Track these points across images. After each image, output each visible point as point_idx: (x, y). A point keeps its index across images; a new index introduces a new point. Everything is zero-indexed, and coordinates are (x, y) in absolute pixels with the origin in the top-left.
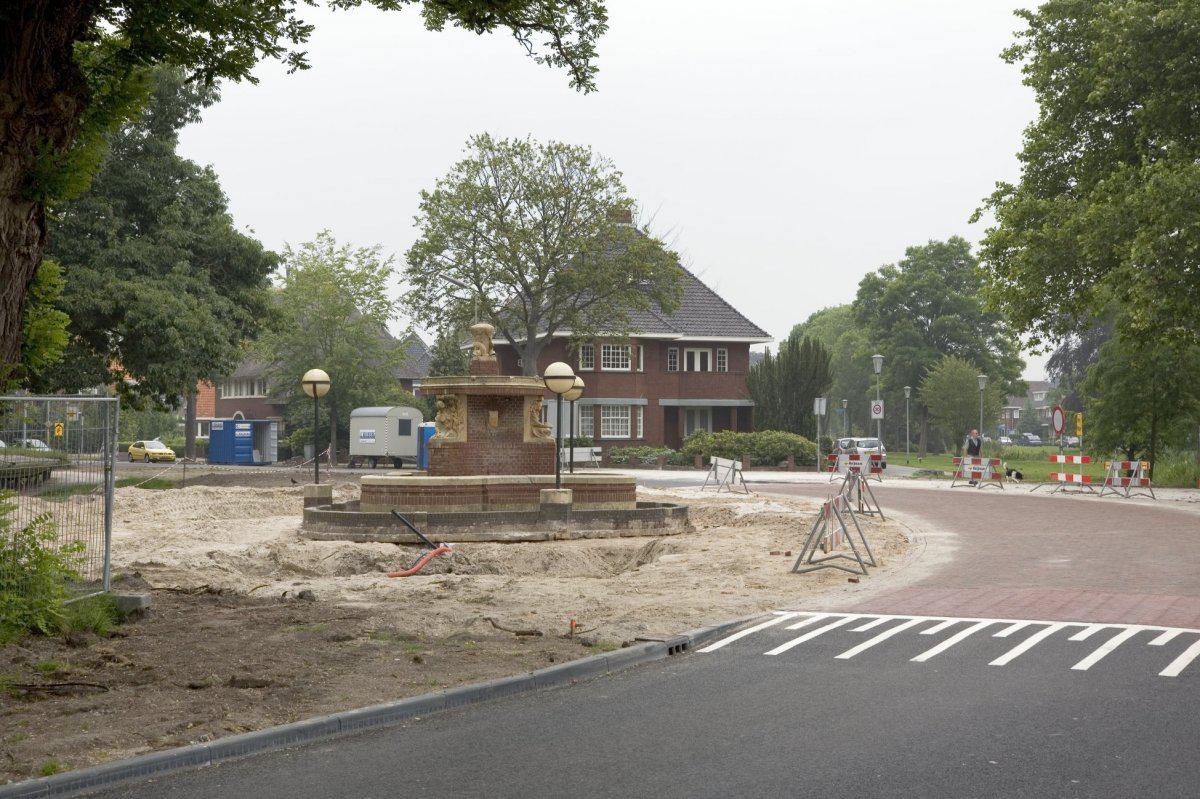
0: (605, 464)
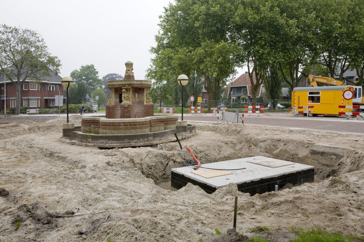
0: (40, 113)
